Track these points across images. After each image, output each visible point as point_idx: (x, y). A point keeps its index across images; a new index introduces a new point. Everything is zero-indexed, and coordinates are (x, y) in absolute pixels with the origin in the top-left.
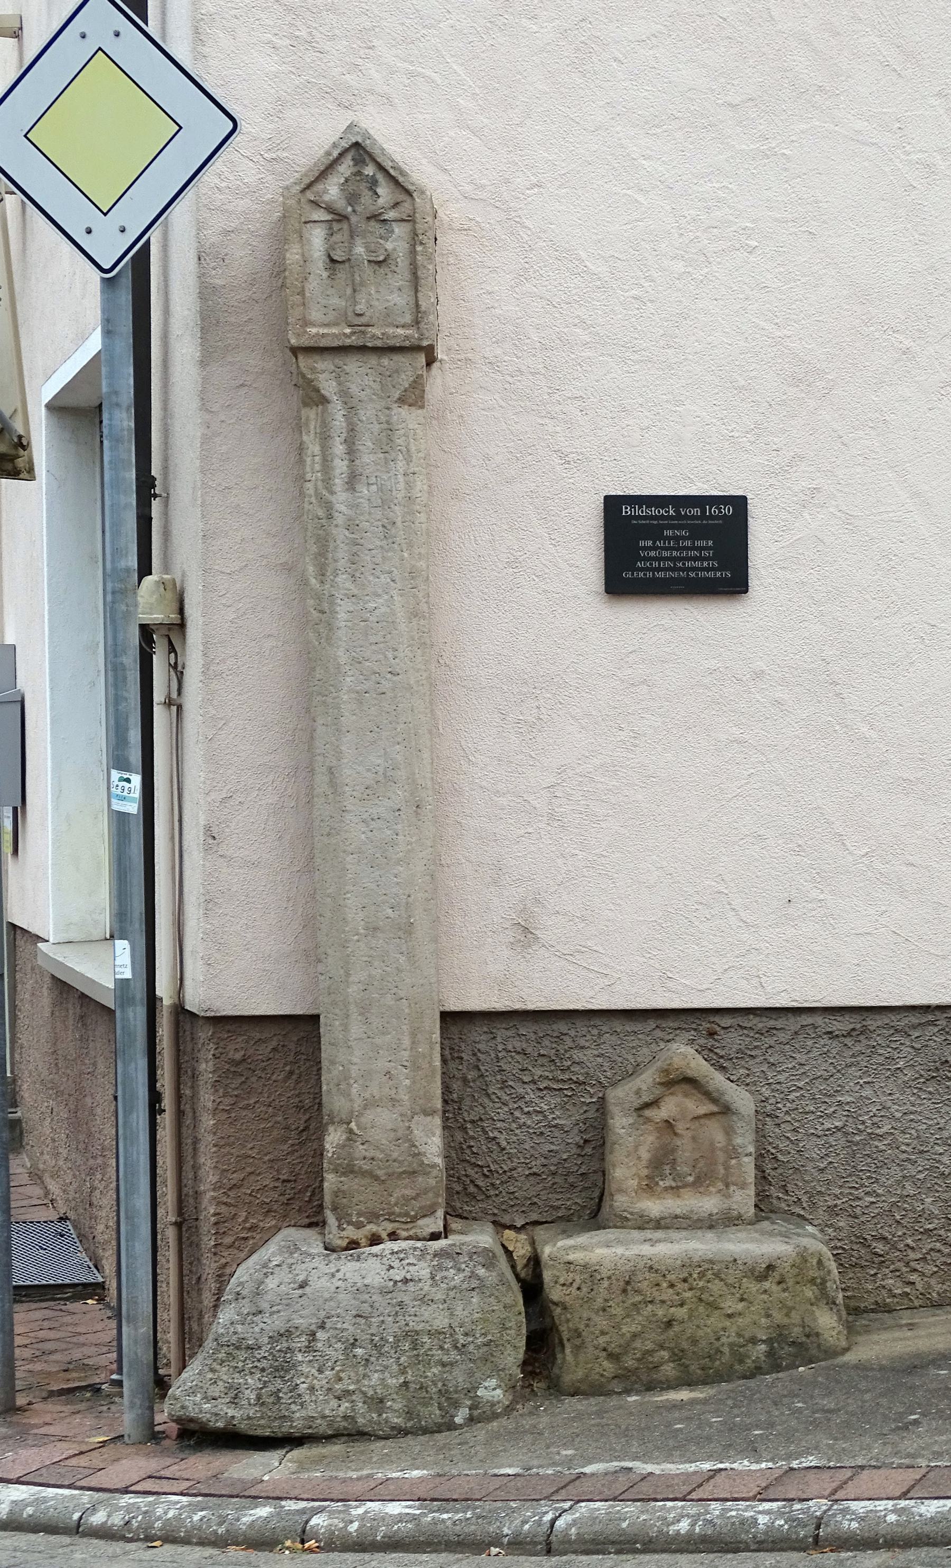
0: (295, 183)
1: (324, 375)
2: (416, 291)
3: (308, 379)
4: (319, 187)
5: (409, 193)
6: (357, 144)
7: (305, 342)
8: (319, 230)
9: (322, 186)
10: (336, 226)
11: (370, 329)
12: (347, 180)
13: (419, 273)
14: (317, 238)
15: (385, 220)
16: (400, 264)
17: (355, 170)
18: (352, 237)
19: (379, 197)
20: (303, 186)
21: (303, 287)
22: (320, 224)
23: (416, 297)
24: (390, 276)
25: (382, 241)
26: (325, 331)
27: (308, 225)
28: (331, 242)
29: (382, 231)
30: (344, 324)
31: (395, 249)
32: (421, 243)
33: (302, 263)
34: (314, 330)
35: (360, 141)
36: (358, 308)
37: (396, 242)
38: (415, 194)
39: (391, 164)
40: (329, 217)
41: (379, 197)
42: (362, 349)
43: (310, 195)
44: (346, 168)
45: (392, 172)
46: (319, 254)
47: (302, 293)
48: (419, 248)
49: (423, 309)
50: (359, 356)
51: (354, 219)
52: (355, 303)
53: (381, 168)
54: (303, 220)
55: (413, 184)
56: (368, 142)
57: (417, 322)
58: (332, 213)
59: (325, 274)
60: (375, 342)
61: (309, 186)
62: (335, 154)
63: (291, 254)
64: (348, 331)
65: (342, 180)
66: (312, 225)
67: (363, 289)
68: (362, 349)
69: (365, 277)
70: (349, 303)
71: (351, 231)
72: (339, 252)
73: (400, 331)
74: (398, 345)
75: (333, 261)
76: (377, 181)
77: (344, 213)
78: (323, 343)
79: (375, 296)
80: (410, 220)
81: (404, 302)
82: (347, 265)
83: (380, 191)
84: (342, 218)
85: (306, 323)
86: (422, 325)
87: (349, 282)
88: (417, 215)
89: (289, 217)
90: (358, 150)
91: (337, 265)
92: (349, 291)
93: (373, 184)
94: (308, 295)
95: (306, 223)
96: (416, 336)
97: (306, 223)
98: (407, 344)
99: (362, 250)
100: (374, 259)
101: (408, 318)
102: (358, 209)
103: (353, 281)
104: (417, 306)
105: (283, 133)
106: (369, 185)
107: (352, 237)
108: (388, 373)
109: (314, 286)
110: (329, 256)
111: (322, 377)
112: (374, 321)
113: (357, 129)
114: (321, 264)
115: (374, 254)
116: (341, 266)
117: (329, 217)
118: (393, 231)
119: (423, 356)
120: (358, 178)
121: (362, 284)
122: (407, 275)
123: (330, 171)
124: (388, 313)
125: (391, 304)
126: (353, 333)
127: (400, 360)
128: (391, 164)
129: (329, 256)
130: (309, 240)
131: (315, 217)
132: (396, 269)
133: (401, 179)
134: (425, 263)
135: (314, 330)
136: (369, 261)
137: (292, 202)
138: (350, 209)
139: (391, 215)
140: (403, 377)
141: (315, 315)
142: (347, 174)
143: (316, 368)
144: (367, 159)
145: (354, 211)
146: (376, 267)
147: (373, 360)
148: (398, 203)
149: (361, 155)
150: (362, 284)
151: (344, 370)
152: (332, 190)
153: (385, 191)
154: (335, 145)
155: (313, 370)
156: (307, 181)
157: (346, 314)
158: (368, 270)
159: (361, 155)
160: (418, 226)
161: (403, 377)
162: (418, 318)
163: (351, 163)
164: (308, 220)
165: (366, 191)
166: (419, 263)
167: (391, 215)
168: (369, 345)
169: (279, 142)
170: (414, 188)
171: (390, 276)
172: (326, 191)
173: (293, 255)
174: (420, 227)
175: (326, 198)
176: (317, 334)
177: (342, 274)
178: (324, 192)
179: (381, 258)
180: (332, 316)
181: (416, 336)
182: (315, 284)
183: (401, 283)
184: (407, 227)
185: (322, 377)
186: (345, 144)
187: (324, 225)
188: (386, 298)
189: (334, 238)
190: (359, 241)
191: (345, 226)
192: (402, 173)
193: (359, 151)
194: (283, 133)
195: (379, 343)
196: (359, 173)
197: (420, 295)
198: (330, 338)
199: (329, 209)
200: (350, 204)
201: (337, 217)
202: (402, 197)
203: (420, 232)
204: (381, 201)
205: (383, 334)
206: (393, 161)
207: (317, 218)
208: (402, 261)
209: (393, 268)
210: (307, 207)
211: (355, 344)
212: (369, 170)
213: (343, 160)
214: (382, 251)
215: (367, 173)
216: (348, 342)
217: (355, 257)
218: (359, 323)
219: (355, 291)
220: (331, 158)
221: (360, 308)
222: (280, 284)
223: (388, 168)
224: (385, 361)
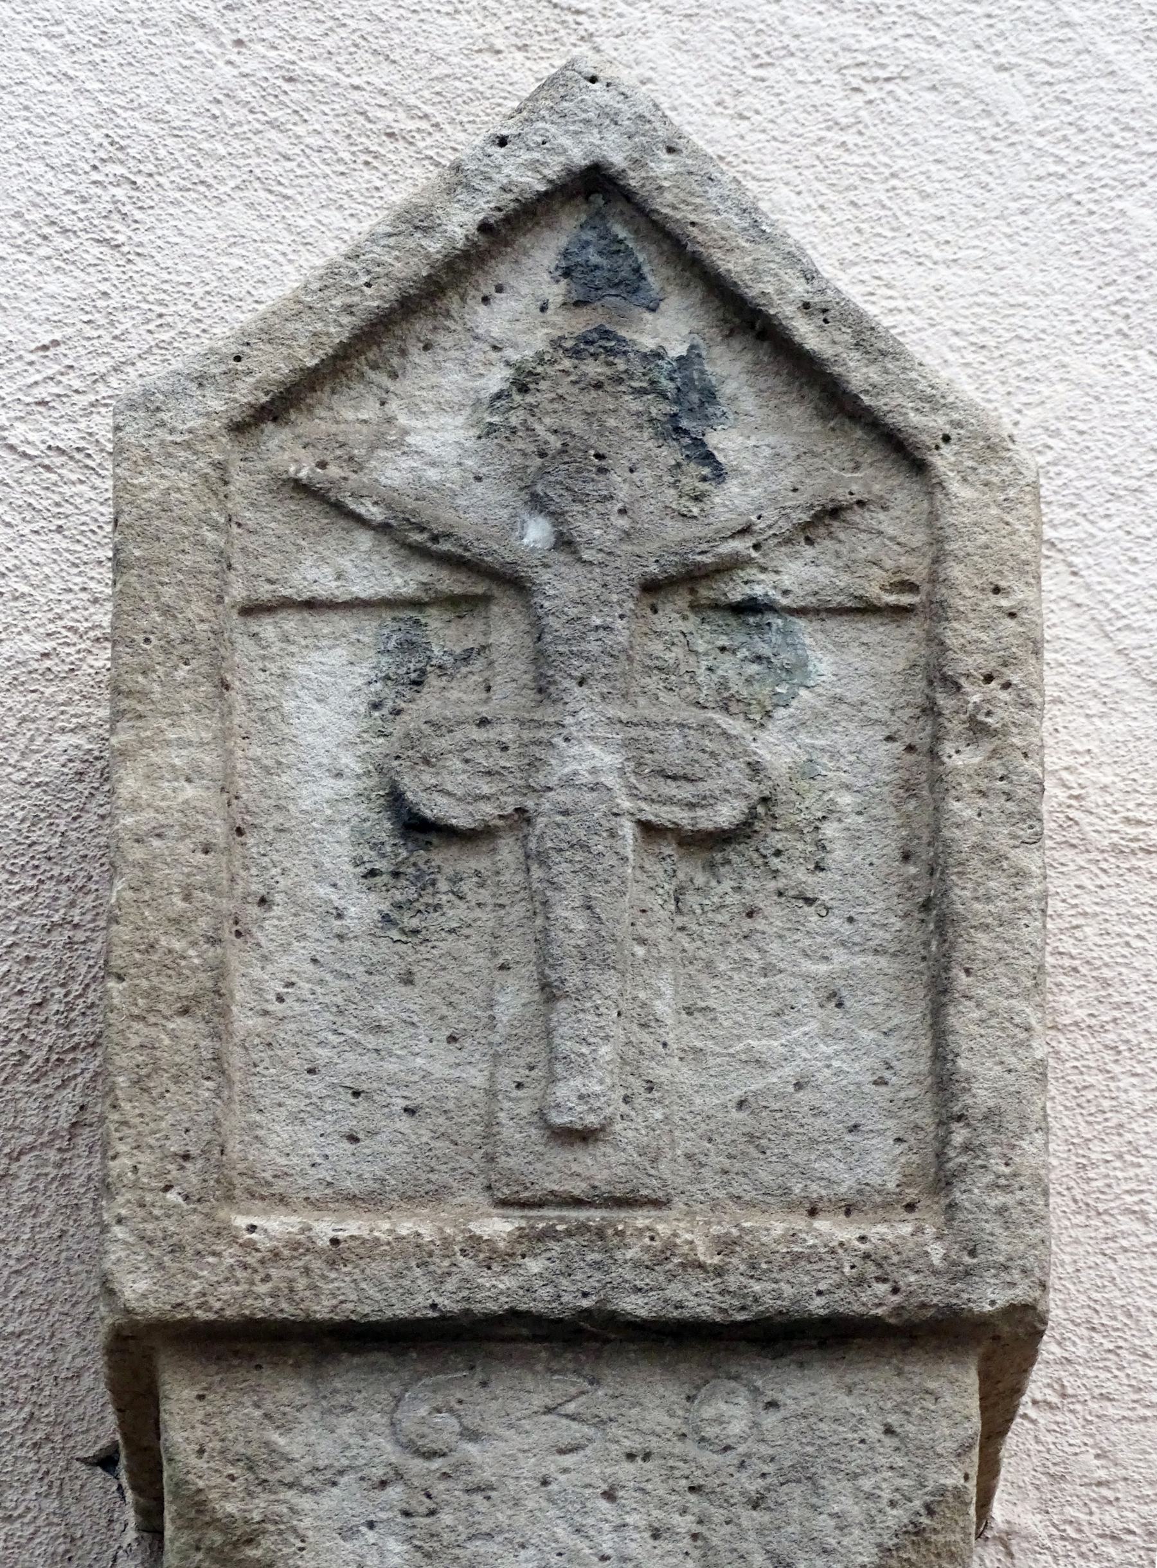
0: (201, 380)
1: (331, 1499)
2: (939, 994)
3: (226, 1525)
4: (350, 413)
5: (904, 453)
6: (594, 185)
7: (214, 1288)
8: (338, 656)
9: (370, 411)
10: (443, 635)
11: (641, 1219)
12: (523, 381)
13: (962, 894)
14: (322, 707)
15: (750, 608)
16: (838, 854)
17: (580, 323)
18: (543, 690)
19: (719, 474)
20: (246, 393)
21: (219, 971)
22: (343, 623)
23: (939, 1033)
24: (775, 916)
25: (735, 726)
26: (354, 1227)
27: (267, 628)
28: (411, 720)
29: (728, 667)
30: (473, 1196)
31: (808, 771)
32: (977, 730)
33: (220, 830)
34: (278, 1225)
35: (617, 159)
36: (564, 1092)
37: (822, 723)
38: (943, 461)
39: (800, 289)
40: (405, 580)
41: (719, 474)
42: (588, 1338)
43: (287, 451)
44: (521, 310)
45: (808, 334)
46: (328, 788)
47: (210, 1003)
48: (962, 758)
49: (981, 1097)
50: (564, 1386)
51: (560, 586)
52: (553, 1063)
53: (745, 319)
54: (238, 592)
55: (932, 401)
56: (664, 166)
57: (939, 1179)
58: (421, 553)
59: (363, 908)
60: (676, 1291)
61: (281, 405)
62: (460, 223)
63: (152, 776)
64: (499, 1227)
65: (497, 379)
66: (291, 622)
67: (610, 983)
68: (588, 1338)
69: (619, 913)
70: (506, 1078)
71: (540, 658)
72: (455, 774)
73: (832, 1229)
74: (817, 1306)
75: (417, 828)
76: (710, 395)
77: (501, 553)
78: (336, 1297)
79: (679, 1033)
80: (910, 604)
81: (859, 1070)
82: (507, 851)
83: (725, 442)
84: (481, 580)
85: (230, 1183)
86: (972, 1193)
87: (516, 948)
88: (955, 571)
89: (147, 563)
90: (597, 220)
91: (445, 860)
92: (514, 999)
93: (684, 413)
94: (244, 1022)
95: (251, 610)
96: (937, 1253)
97: (251, 610)
98: (876, 1299)
99: (608, 759)
100: (682, 817)
101: (882, 1163)
102: (587, 526)
103: (543, 940)
104: (944, 1081)
105: (125, 322)
106: (660, 409)
107: (543, 690)
108: (754, 1486)
109: (279, 970)
110: (395, 800)
111: (314, 1511)
112: (672, 1172)
113: (598, 94)
114: (338, 852)
115: (686, 791)
116: (472, 862)
117: (405, 580)
118: (795, 671)
119: (971, 1380)
120: (594, 369)
121: (598, 954)
122: (883, 915)
123: (421, 326)
124: (759, 1127)
125: (780, 1077)
126: (534, 1240)
127: (825, 1400)
128: (800, 289)
129: (395, 800)
130: (267, 715)
131: (314, 576)
132: (811, 882)
133: (859, 374)
134: (1001, 839)
135: (278, 1225)
136: (649, 830)
137: (170, 482)
138: (537, 532)
139: (794, 575)
140: (846, 1504)
141: (288, 1138)
142: (531, 343)
143: (277, 1457)
144: (646, 257)
145: (564, 543)
146: (691, 870)
147: (651, 1404)
148: (834, 512)
149: (615, 249)
150: (598, 954)
151: (466, 1466)
152: (429, 433)
153: (760, 452)
154: (458, 179)
155: (263, 1470)
156: (272, 367)
157: (490, 1124)
158: (640, 884)
159: (615, 249)
160: (957, 633)
161: (846, 1504)
162: (951, 1138)
163: (555, 292)
164: (264, 592)
165: (646, 441)
166: (964, 839)
167: (794, 575)
168: (635, 1306)
169: (101, 365)
170: (939, 422)
171: (775, 916)
172: (387, 438)
173: (168, 782)
174: (969, 639)
175: (393, 472)
176: (299, 1246)
177: (475, 897)
178: (378, 443)
179: (726, 814)
180: (395, 1146)
181: (937, 1253)
182: (294, 961)
183: (840, 957)
184: (890, 649)
185: (314, 1511)
186: (522, 172)
187: (369, 628)
188: (735, 1077)
189: (432, 701)
190: (585, 708)
191: (504, 631)
192: (866, 337)
193: (603, 214)
194: (125, 322)
195: (698, 1300)
196: (600, 342)
197: (963, 1020)
198: (380, 1268)
199: (409, 533)
200: (538, 503)
201: (449, 582)
202: (870, 477)
203: (969, 663)
204: (731, 501)
205: (726, 1245)
206: (809, 276)
207: (326, 586)
208: (855, 838)
209: (800, 875)
210: (273, 521)
211: (540, 1301)
212: (669, 327)
213: (502, 270)
214: (736, 771)
215: (648, 343)
216: (496, 1290)
217: (564, 797)
218: (564, 1173)
219: (550, 992)
220: (434, 246)
221: (570, 1099)
222: (65, 1112)
223: (786, 311)
224: (731, 1411)
